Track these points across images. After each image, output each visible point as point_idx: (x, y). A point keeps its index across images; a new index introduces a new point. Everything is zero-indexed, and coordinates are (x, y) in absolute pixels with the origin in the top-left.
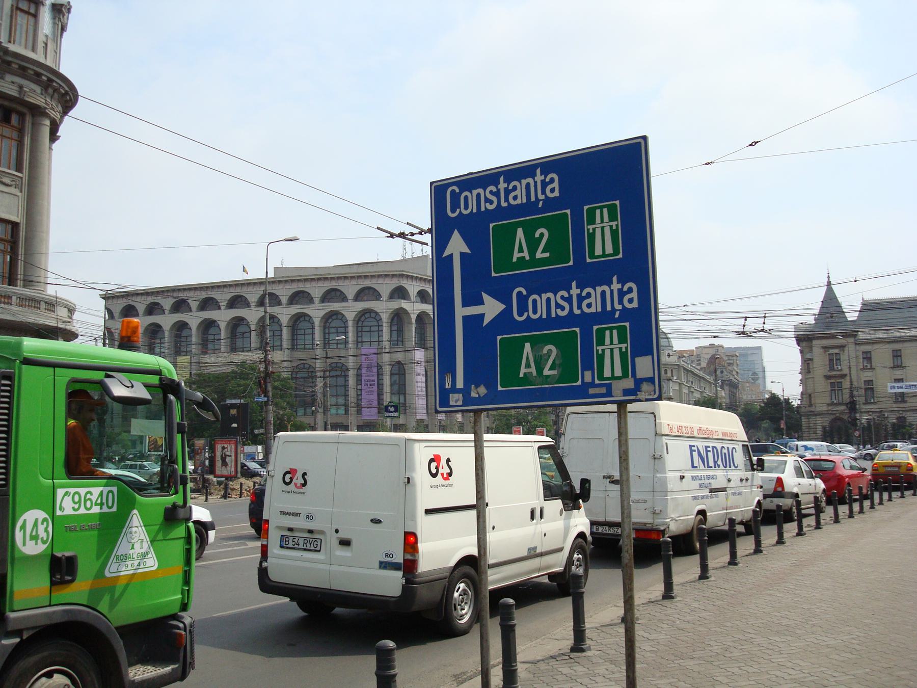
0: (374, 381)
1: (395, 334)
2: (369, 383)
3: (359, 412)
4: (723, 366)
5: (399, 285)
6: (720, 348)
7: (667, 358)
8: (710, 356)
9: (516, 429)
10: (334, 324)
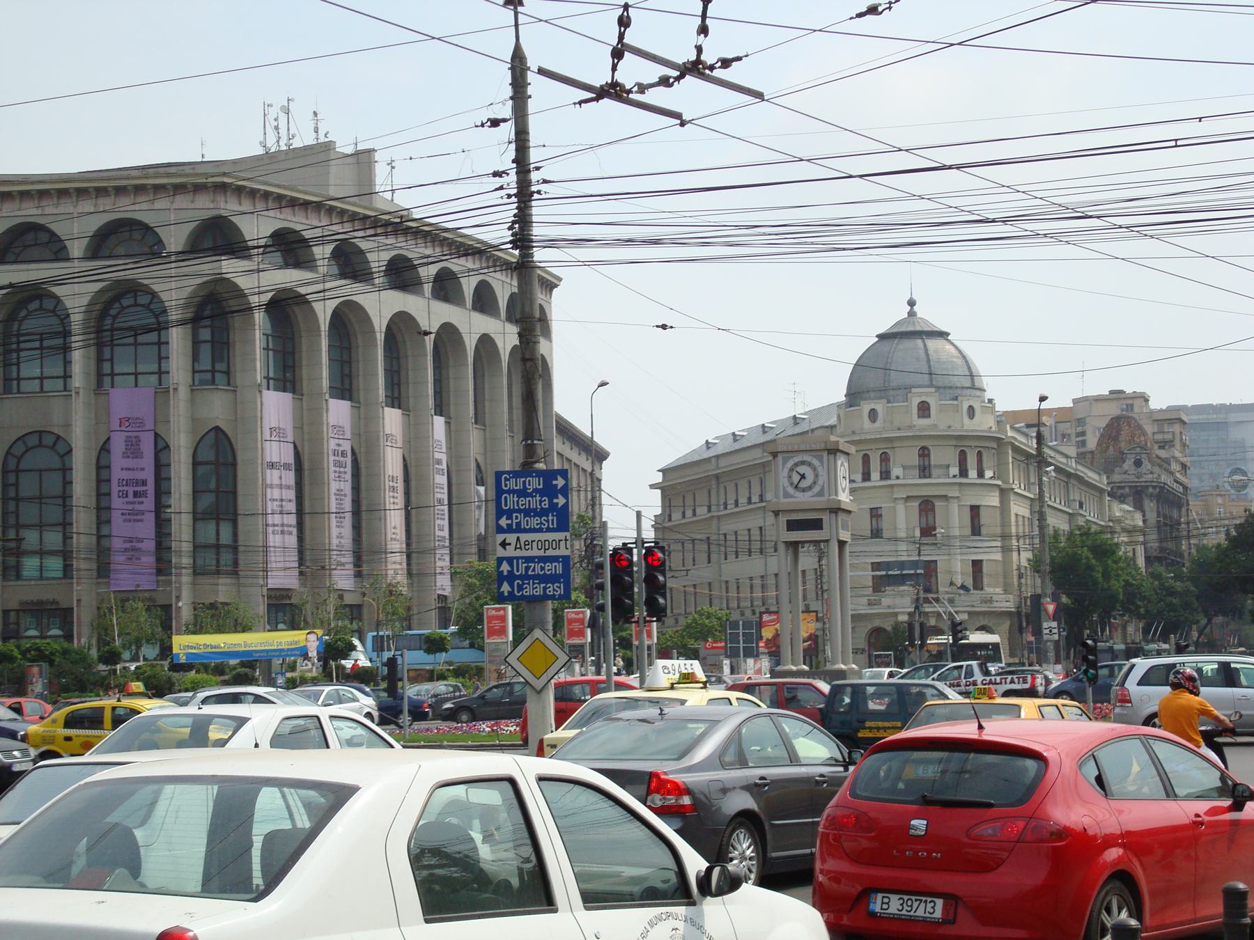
0: (144, 483)
1: (206, 351)
2: (131, 490)
3: (103, 570)
4: (1142, 448)
5: (215, 213)
6: (1137, 403)
7: (966, 420)
8: (1107, 422)
9: (494, 613)
10: (31, 325)
